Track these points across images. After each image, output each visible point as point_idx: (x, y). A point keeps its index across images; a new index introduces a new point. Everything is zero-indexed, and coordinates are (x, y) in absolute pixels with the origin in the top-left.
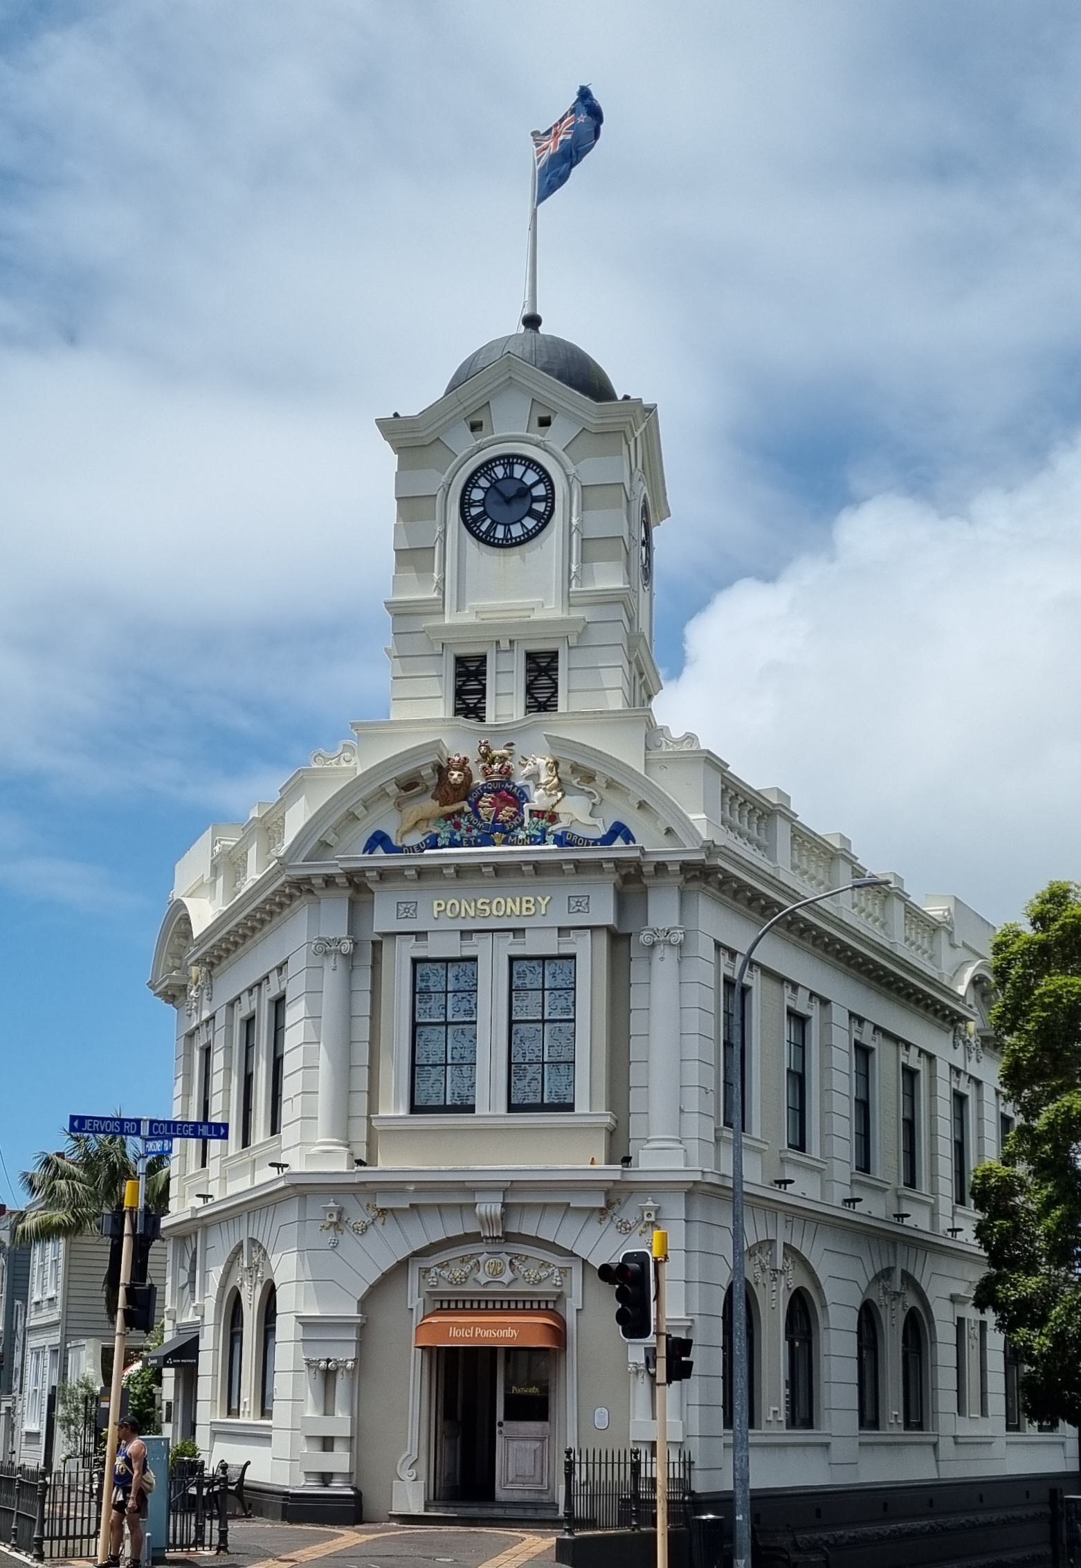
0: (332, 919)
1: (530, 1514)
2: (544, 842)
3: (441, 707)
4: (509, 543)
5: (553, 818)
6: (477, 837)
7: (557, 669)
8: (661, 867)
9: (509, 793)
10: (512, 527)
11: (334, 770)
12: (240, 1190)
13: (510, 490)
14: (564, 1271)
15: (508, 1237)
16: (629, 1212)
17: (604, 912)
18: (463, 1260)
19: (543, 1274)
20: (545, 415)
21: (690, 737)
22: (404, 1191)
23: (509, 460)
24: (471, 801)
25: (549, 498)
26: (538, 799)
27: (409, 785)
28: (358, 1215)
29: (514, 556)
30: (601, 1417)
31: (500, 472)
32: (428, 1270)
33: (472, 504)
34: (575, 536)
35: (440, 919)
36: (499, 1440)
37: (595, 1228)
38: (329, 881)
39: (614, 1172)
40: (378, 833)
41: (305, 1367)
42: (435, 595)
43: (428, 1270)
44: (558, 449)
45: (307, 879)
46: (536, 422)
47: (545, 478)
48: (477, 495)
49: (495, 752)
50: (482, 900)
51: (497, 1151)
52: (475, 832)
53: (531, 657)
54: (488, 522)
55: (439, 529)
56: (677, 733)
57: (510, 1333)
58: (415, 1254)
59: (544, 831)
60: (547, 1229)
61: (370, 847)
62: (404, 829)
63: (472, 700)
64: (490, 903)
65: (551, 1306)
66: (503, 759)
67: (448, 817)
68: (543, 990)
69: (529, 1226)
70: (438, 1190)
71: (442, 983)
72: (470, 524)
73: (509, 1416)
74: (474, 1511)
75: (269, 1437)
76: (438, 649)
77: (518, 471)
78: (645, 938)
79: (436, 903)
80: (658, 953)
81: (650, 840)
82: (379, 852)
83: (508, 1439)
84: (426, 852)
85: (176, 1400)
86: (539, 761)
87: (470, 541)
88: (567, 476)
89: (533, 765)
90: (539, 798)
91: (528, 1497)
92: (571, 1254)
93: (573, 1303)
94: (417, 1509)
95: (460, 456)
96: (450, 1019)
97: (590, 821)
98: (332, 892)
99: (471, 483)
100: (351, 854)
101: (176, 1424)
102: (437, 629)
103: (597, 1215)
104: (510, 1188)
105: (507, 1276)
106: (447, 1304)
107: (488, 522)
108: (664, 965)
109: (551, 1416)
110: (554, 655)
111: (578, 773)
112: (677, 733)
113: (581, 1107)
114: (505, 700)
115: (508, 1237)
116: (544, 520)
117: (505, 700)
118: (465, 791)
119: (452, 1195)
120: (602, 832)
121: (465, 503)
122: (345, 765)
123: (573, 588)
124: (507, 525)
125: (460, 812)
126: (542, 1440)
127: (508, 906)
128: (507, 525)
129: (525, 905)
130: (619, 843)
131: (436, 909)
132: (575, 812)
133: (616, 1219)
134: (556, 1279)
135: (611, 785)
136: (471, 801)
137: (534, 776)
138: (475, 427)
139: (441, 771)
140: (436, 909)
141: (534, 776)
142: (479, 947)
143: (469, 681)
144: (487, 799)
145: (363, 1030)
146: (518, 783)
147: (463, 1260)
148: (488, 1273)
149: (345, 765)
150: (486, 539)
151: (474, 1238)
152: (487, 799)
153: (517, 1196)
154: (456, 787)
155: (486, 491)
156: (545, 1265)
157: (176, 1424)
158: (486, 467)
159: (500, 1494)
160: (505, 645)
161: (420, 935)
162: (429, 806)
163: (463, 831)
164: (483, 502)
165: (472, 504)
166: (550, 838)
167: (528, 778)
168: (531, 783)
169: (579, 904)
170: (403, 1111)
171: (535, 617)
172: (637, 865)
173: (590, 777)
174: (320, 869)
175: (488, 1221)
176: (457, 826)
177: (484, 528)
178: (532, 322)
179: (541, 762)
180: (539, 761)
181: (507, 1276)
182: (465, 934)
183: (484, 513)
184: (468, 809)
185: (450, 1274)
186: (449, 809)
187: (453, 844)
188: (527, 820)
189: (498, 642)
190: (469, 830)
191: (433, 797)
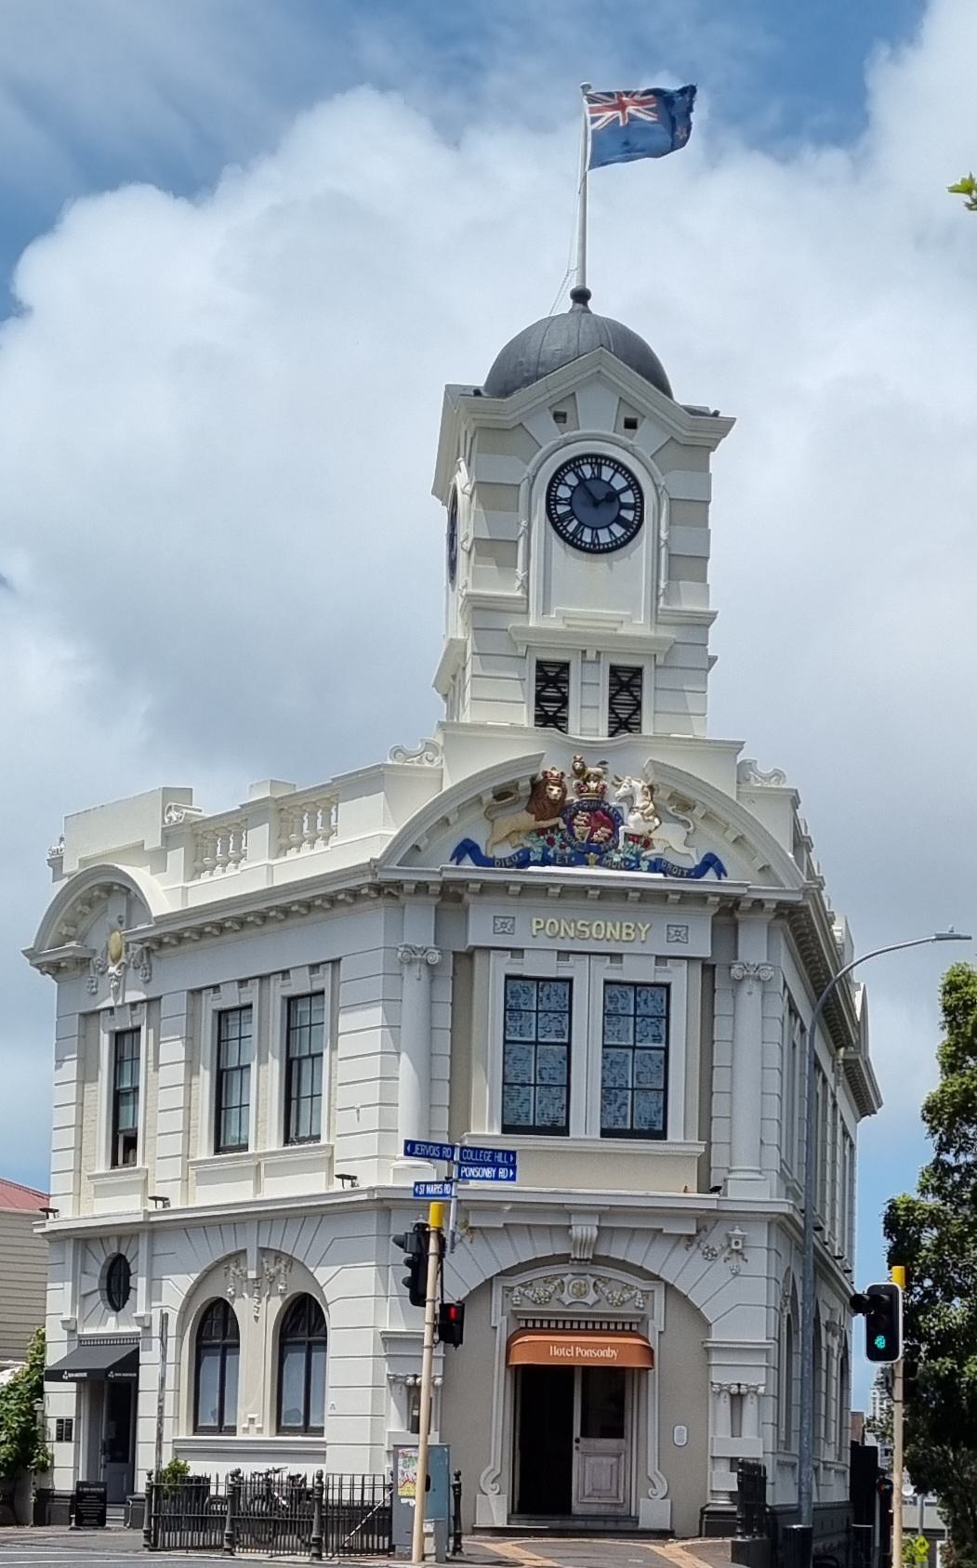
0: (419, 928)
1: (610, 1526)
2: (637, 868)
3: (524, 715)
4: (595, 550)
5: (647, 844)
6: (571, 855)
7: (640, 686)
8: (759, 904)
9: (606, 814)
10: (600, 532)
11: (417, 769)
13: (600, 494)
15: (597, 1260)
16: (715, 1239)
17: (700, 943)
18: (547, 1280)
19: (626, 1296)
21: (778, 774)
22: (498, 1211)
23: (598, 460)
24: (560, 817)
25: (638, 507)
26: (632, 823)
27: (502, 794)
29: (600, 565)
30: (680, 1435)
31: (587, 471)
32: (512, 1289)
33: (557, 501)
34: (663, 551)
35: (537, 941)
36: (576, 1456)
37: (680, 1255)
38: (422, 888)
39: (710, 1201)
40: (467, 840)
41: (385, 1382)
42: (519, 594)
43: (512, 1289)
45: (399, 885)
47: (634, 485)
48: (564, 492)
49: (590, 769)
51: (580, 1172)
52: (568, 850)
53: (614, 670)
54: (575, 523)
55: (524, 523)
56: (764, 768)
57: (610, 1353)
59: (638, 855)
60: (635, 1253)
61: (458, 855)
62: (496, 839)
63: (551, 708)
65: (630, 1327)
66: (598, 777)
67: (541, 832)
68: (635, 1016)
69: (618, 1250)
70: (537, 1211)
72: (556, 522)
73: (585, 1433)
74: (556, 1524)
75: (324, 1454)
76: (522, 651)
77: (607, 473)
78: (736, 972)
80: (746, 987)
81: (740, 876)
82: (468, 863)
83: (586, 1454)
84: (532, 869)
85: (78, 1417)
86: (634, 783)
87: (556, 542)
88: (656, 486)
89: (628, 789)
90: (636, 822)
91: (603, 1510)
92: (657, 1278)
93: (656, 1324)
94: (501, 1522)
95: (545, 448)
96: (630, 1052)
97: (684, 850)
98: (421, 899)
99: (557, 479)
100: (439, 866)
101: (77, 1442)
102: (518, 631)
103: (683, 1242)
104: (604, 1212)
105: (591, 1298)
106: (528, 1324)
107: (575, 523)
108: (750, 999)
109: (627, 1432)
110: (638, 672)
111: (677, 802)
112: (764, 768)
113: (675, 1133)
114: (588, 716)
115: (597, 1260)
116: (633, 529)
117: (588, 716)
118: (560, 808)
119: (558, 1215)
120: (696, 861)
121: (552, 501)
122: (427, 765)
123: (661, 605)
125: (554, 828)
126: (618, 1456)
127: (606, 930)
130: (710, 876)
131: (535, 927)
132: (671, 841)
133: (703, 1245)
134: (639, 1301)
135: (707, 817)
136: (560, 817)
137: (629, 798)
138: (560, 417)
139: (538, 786)
140: (535, 927)
141: (629, 798)
143: (551, 691)
144: (582, 818)
145: (444, 1043)
146: (613, 804)
147: (547, 1280)
148: (574, 1294)
149: (427, 765)
150: (573, 541)
151: (565, 1259)
152: (582, 818)
153: (613, 1219)
154: (553, 803)
155: (573, 489)
156: (628, 1287)
157: (77, 1442)
158: (573, 464)
159: (577, 1508)
160: (591, 655)
161: (517, 952)
162: (527, 820)
163: (556, 847)
164: (570, 502)
165: (557, 501)
166: (644, 865)
167: (622, 799)
168: (624, 805)
169: (679, 935)
170: (497, 1132)
171: (621, 632)
172: (736, 901)
173: (686, 806)
174: (410, 875)
175: (583, 1244)
176: (551, 842)
177: (571, 528)
178: (581, 296)
179: (638, 785)
180: (634, 783)
181: (591, 1298)
182: (564, 955)
183: (572, 513)
184: (563, 826)
185: (533, 1294)
186: (544, 824)
187: (545, 861)
188: (622, 843)
189: (584, 652)
190: (562, 847)
191: (528, 809)
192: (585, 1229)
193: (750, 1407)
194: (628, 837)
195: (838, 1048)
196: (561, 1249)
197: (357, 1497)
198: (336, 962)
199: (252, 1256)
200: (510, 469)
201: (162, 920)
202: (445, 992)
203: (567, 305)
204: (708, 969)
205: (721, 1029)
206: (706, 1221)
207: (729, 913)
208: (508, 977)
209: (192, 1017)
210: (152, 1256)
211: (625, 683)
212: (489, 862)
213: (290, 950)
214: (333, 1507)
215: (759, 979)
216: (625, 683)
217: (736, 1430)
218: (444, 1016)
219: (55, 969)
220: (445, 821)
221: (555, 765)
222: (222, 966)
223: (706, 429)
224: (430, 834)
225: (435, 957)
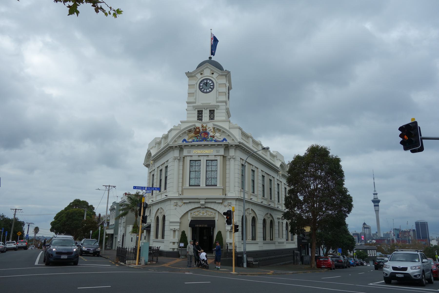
3: (196, 119)
4: (206, 93)
8: (232, 145)
14: (215, 213)
15: (206, 207)
25: (213, 86)
27: (190, 131)
28: (180, 203)
38: (176, 147)
44: (215, 78)
45: (172, 147)
47: (213, 82)
48: (202, 85)
58: (190, 210)
63: (200, 118)
67: (196, 137)
69: (209, 205)
80: (231, 159)
81: (229, 141)
82: (185, 142)
108: (232, 161)
111: (217, 129)
115: (206, 207)
116: (212, 89)
118: (199, 132)
121: (200, 86)
127: (206, 151)
130: (225, 141)
134: (214, 215)
138: (201, 74)
142: (201, 158)
151: (200, 207)
154: (197, 132)
164: (202, 86)
175: (202, 205)
181: (205, 214)
192: (202, 202)
193: (177, 232)
194: (211, 136)
197: (331, 251)
200: (193, 82)
202: (181, 163)
203: (208, 59)
204: (224, 157)
205: (227, 167)
206: (224, 199)
207: (227, 147)
208: (207, 160)
209: (158, 169)
211: (212, 112)
212: (188, 142)
214: (155, 250)
216: (212, 112)
217: (174, 236)
218: (181, 168)
220: (180, 136)
221: (199, 125)
224: (177, 138)
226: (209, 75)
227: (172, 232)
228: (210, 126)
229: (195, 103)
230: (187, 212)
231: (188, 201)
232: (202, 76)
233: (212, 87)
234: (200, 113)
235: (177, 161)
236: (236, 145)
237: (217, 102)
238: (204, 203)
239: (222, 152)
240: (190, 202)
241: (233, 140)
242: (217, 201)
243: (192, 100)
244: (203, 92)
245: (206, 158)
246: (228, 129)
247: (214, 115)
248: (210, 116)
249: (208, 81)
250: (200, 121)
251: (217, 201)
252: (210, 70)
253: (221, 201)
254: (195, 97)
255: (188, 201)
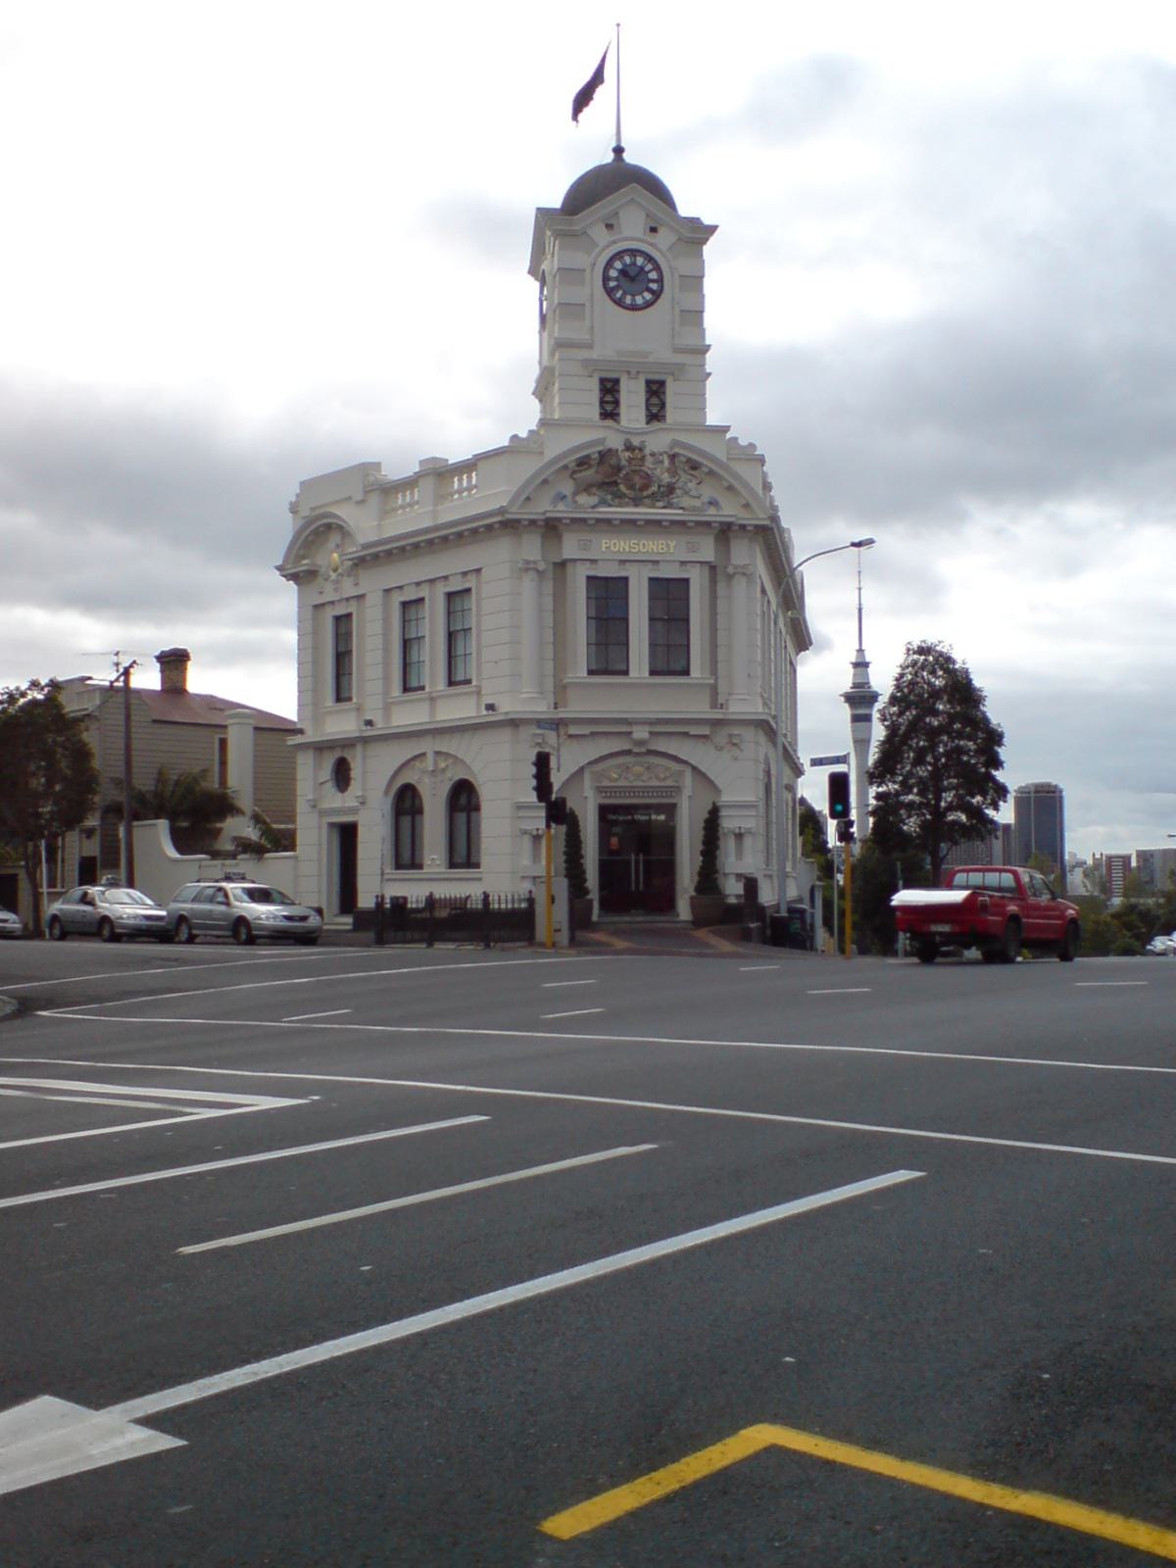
0: (531, 548)
3: (594, 412)
4: (634, 308)
8: (743, 527)
12: (401, 724)
14: (681, 773)
15: (650, 752)
20: (653, 225)
27: (583, 463)
38: (533, 522)
44: (664, 248)
45: (518, 521)
46: (648, 229)
50: (633, 542)
58: (590, 763)
63: (609, 408)
64: (638, 545)
69: (662, 745)
71: (608, 595)
78: (730, 570)
79: (604, 541)
80: (737, 576)
108: (740, 586)
115: (650, 752)
116: (657, 295)
119: (621, 726)
121: (606, 279)
124: (625, 293)
128: (633, 295)
129: (660, 546)
138: (609, 227)
151: (628, 752)
161: (594, 561)
164: (616, 279)
175: (641, 743)
178: (618, 151)
195: (788, 611)
196: (626, 747)
198: (478, 571)
199: (430, 757)
201: (365, 547)
204: (713, 568)
206: (717, 724)
209: (386, 606)
210: (364, 758)
211: (655, 390)
213: (450, 564)
215: (744, 574)
217: (536, 857)
219: (294, 577)
220: (545, 482)
221: (615, 442)
222: (407, 574)
223: (698, 233)
225: (541, 566)
226: (640, 235)
227: (527, 842)
228: (657, 442)
229: (590, 346)
230: (582, 770)
231: (585, 730)
232: (650, 237)
233: (654, 286)
234: (609, 390)
235: (532, 575)
236: (756, 527)
237: (677, 350)
238: (646, 735)
239: (707, 550)
240: (592, 734)
241: (747, 506)
242: (693, 731)
243: (577, 332)
244: (619, 303)
245: (442, 589)
246: (725, 460)
247: (647, 409)
248: (648, 406)
249: (640, 261)
250: (609, 423)
251: (693, 730)
252: (644, 215)
253: (705, 731)
254: (587, 323)
255: (585, 730)
